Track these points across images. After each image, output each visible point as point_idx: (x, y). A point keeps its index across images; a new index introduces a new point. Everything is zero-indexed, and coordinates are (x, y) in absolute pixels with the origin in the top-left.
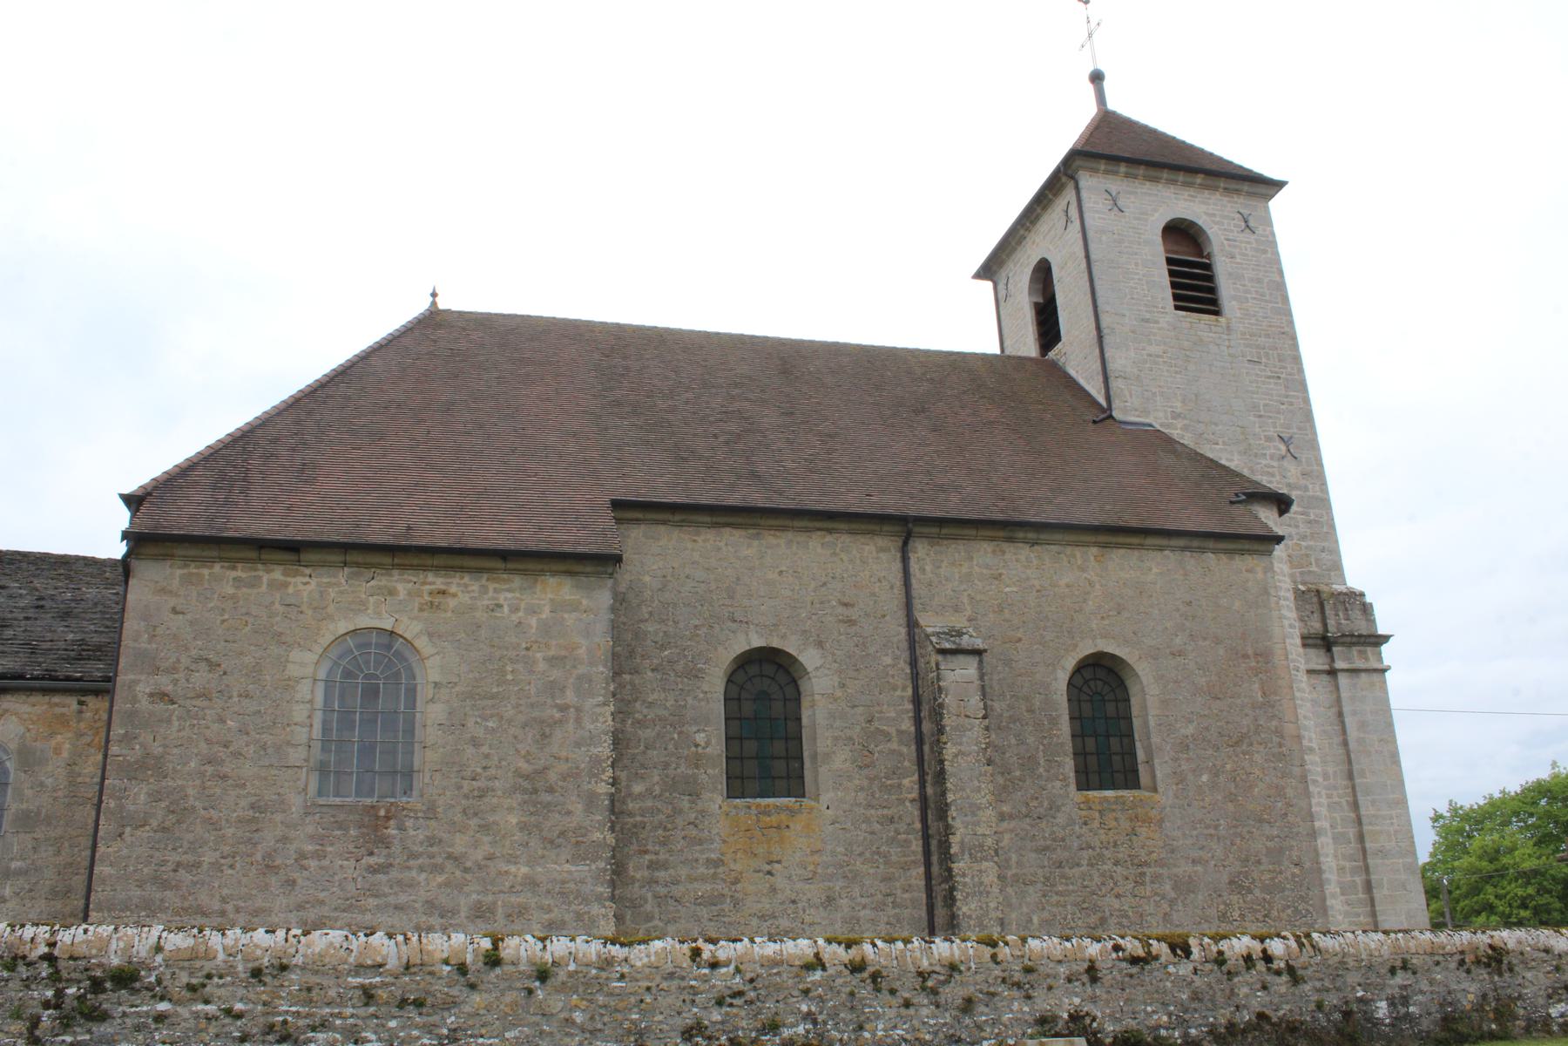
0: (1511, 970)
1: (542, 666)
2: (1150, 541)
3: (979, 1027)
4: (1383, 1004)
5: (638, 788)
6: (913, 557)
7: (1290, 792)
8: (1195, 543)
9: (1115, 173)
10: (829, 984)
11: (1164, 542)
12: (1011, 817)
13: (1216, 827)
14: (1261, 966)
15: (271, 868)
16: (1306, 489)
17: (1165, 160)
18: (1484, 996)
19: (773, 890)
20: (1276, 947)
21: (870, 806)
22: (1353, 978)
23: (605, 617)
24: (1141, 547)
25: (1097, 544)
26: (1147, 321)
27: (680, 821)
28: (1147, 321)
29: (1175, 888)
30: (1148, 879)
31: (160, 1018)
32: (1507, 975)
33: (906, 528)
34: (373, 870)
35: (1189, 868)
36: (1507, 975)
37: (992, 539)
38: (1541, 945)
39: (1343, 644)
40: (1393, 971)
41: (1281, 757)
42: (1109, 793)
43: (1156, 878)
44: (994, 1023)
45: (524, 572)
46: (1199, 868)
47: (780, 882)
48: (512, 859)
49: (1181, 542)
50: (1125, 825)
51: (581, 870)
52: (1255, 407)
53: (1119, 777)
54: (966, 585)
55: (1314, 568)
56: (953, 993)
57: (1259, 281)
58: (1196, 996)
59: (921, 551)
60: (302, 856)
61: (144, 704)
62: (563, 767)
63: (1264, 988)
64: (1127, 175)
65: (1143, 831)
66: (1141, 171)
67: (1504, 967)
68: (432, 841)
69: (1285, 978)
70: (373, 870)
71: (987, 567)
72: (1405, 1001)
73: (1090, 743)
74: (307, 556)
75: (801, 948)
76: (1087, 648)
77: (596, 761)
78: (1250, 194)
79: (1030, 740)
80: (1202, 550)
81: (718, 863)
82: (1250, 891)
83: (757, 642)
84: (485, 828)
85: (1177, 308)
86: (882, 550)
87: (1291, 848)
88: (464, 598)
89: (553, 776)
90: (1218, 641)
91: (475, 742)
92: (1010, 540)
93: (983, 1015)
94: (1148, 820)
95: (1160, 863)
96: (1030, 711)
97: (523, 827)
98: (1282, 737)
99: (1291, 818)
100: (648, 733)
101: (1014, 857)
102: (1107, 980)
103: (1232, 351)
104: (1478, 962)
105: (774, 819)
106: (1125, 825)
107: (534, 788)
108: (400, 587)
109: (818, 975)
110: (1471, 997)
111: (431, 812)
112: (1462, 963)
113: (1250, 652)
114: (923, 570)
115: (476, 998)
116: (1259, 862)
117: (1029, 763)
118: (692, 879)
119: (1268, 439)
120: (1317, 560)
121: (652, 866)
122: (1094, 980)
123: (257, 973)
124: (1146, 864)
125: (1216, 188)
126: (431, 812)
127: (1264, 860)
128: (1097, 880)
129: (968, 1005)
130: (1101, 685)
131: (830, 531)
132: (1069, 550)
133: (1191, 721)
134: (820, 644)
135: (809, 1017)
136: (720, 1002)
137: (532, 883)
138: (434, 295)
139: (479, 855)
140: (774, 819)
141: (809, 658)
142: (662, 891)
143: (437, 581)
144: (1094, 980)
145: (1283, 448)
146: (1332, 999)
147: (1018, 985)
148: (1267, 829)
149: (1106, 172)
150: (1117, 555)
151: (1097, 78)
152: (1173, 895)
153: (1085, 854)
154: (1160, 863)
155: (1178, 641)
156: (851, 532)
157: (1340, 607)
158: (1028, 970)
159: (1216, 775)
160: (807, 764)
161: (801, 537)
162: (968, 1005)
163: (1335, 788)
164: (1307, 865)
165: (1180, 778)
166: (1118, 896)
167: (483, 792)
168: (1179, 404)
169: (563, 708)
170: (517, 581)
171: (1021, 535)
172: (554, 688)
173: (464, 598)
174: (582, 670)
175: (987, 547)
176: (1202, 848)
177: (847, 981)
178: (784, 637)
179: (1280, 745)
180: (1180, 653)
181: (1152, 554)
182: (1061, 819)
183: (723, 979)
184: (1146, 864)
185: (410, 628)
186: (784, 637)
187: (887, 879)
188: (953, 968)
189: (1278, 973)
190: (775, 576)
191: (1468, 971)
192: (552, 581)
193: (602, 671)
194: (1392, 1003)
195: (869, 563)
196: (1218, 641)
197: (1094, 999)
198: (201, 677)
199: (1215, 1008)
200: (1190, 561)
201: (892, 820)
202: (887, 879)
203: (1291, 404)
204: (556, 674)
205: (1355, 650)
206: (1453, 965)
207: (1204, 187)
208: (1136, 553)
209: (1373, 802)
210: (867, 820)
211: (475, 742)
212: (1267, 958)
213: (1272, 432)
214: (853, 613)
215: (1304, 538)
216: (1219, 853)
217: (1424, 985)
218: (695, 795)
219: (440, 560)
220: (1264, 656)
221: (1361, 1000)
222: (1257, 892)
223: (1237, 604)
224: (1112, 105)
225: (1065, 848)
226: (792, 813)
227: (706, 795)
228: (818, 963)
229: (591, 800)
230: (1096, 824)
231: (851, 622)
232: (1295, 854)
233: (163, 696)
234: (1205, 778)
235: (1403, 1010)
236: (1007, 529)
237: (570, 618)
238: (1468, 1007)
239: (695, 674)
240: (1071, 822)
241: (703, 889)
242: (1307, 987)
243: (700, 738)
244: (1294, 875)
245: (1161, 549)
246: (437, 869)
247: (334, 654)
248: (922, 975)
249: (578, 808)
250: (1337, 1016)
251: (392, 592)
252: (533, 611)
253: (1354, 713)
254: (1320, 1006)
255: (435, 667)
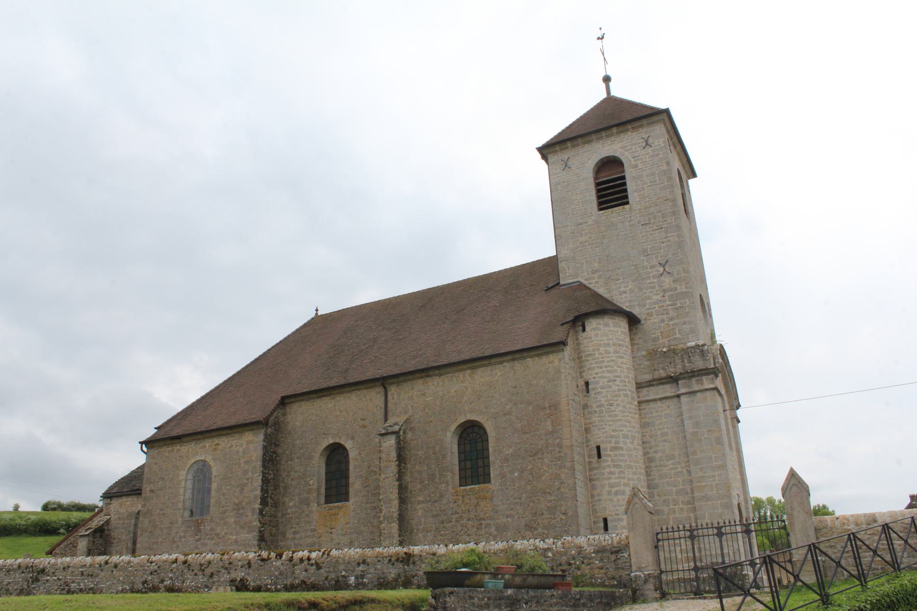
0: (414, 563)
1: (243, 465)
2: (492, 361)
3: (214, 583)
4: (353, 578)
5: (291, 504)
6: (389, 394)
7: (563, 476)
8: (517, 356)
9: (567, 148)
10: (177, 568)
11: (501, 359)
12: (423, 502)
13: (520, 499)
14: (306, 562)
15: (174, 542)
16: (676, 289)
17: (576, 134)
18: (399, 575)
19: (332, 540)
20: (314, 555)
21: (367, 503)
22: (341, 567)
23: (262, 443)
24: (490, 364)
25: (468, 368)
26: (581, 224)
27: (303, 515)
28: (581, 224)
29: (497, 529)
30: (483, 526)
31: (47, 580)
32: (411, 566)
33: (384, 382)
34: (197, 541)
35: (505, 520)
36: (411, 566)
37: (422, 378)
38: (431, 552)
39: (684, 378)
40: (359, 564)
41: (559, 458)
42: (477, 487)
43: (488, 526)
44: (218, 581)
45: (238, 432)
46: (510, 519)
47: (334, 536)
48: (231, 534)
49: (509, 357)
50: (474, 501)
51: (249, 536)
52: (645, 251)
53: (481, 478)
54: (409, 400)
55: (678, 336)
56: (208, 571)
57: (653, 174)
58: (281, 574)
59: (393, 390)
60: (181, 537)
61: (148, 494)
62: (246, 500)
63: (306, 571)
64: (573, 146)
65: (483, 503)
66: (604, 134)
67: (411, 562)
68: (212, 529)
69: (314, 567)
70: (197, 541)
71: (420, 391)
72: (363, 577)
73: (468, 464)
74: (184, 439)
75: (174, 556)
76: (462, 420)
77: (256, 496)
78: (649, 124)
79: (433, 466)
80: (524, 358)
81: (314, 530)
82: (536, 529)
83: (331, 441)
84: (225, 524)
85: (601, 209)
86: (378, 393)
87: (561, 506)
88: (223, 445)
89: (244, 503)
90: (529, 403)
91: (224, 495)
92: (428, 376)
93: (215, 578)
94: (485, 498)
95: (491, 518)
96: (435, 453)
97: (235, 522)
98: (561, 447)
99: (562, 490)
100: (294, 483)
101: (423, 520)
102: (253, 567)
103: (632, 223)
104: (397, 560)
105: (333, 512)
106: (474, 501)
107: (238, 507)
108: (207, 445)
109: (175, 565)
110: (393, 575)
111: (211, 521)
112: (390, 560)
113: (547, 405)
114: (393, 398)
115: (103, 574)
116: (542, 514)
117: (432, 477)
118: (306, 537)
119: (652, 267)
120: (679, 330)
121: (294, 533)
122: (250, 567)
123: (64, 568)
124: (483, 519)
125: (627, 130)
126: (211, 521)
127: (545, 513)
128: (459, 528)
129: (212, 575)
130: (472, 437)
131: (359, 390)
132: (457, 374)
133: (511, 447)
134: (353, 438)
135: (171, 578)
136: (151, 574)
137: (236, 541)
138: (317, 310)
139: (223, 533)
140: (333, 512)
141: (348, 445)
142: (296, 542)
143: (216, 441)
144: (250, 567)
145: (661, 269)
146: (333, 576)
147: (226, 569)
148: (549, 498)
149: (561, 150)
150: (480, 371)
151: (607, 79)
152: (496, 533)
153: (454, 516)
154: (491, 518)
155: (508, 407)
156: (367, 388)
157: (686, 356)
158: (230, 563)
159: (522, 472)
160: (323, 491)
161: (349, 395)
162: (212, 575)
163: (679, 463)
164: (570, 513)
165: (503, 476)
166: (468, 535)
167: (225, 512)
168: (596, 265)
169: (247, 479)
170: (237, 436)
171: (431, 373)
172: (246, 472)
173: (223, 445)
174: (254, 464)
175: (420, 381)
176: (512, 509)
177: (182, 567)
178: (340, 438)
179: (560, 452)
180: (509, 413)
181: (497, 366)
182: (445, 501)
183: (153, 567)
184: (483, 519)
185: (209, 459)
186: (340, 438)
187: (372, 533)
188: (210, 562)
189: (312, 565)
190: (338, 413)
191: (393, 564)
192: (247, 434)
193: (260, 463)
194: (357, 578)
195: (372, 399)
196: (529, 403)
197: (248, 574)
198: (160, 483)
199: (287, 578)
200: (517, 365)
201: (375, 508)
202: (372, 533)
203: (669, 241)
204: (247, 467)
205: (694, 380)
206: (386, 561)
207: (618, 133)
208: (489, 368)
209: (701, 469)
210: (366, 509)
211: (224, 495)
212: (309, 559)
213: (655, 262)
214: (366, 422)
215: (672, 319)
216: (521, 511)
217: (372, 570)
218: (308, 505)
219: (214, 434)
220: (555, 406)
221: (343, 576)
222: (540, 530)
223: (542, 381)
224: (613, 93)
225: (445, 515)
226: (340, 508)
227: (312, 504)
228: (176, 561)
229: (253, 510)
230: (460, 502)
231: (364, 426)
232: (563, 508)
233: (152, 491)
234: (516, 474)
235: (360, 580)
236: (425, 372)
237: (251, 446)
238: (391, 579)
239: (310, 458)
240: (449, 502)
241: (309, 541)
242: (322, 571)
243: (311, 482)
244: (561, 519)
245: (501, 363)
246: (213, 539)
247: (195, 467)
248: (201, 565)
249: (250, 514)
250: (333, 582)
251: (205, 447)
252: (241, 446)
253: (691, 418)
254: (326, 578)
255: (216, 469)
